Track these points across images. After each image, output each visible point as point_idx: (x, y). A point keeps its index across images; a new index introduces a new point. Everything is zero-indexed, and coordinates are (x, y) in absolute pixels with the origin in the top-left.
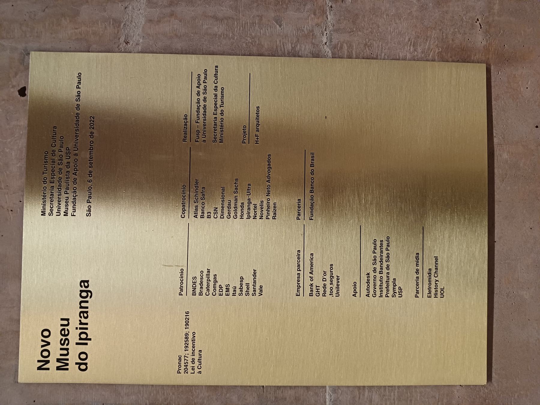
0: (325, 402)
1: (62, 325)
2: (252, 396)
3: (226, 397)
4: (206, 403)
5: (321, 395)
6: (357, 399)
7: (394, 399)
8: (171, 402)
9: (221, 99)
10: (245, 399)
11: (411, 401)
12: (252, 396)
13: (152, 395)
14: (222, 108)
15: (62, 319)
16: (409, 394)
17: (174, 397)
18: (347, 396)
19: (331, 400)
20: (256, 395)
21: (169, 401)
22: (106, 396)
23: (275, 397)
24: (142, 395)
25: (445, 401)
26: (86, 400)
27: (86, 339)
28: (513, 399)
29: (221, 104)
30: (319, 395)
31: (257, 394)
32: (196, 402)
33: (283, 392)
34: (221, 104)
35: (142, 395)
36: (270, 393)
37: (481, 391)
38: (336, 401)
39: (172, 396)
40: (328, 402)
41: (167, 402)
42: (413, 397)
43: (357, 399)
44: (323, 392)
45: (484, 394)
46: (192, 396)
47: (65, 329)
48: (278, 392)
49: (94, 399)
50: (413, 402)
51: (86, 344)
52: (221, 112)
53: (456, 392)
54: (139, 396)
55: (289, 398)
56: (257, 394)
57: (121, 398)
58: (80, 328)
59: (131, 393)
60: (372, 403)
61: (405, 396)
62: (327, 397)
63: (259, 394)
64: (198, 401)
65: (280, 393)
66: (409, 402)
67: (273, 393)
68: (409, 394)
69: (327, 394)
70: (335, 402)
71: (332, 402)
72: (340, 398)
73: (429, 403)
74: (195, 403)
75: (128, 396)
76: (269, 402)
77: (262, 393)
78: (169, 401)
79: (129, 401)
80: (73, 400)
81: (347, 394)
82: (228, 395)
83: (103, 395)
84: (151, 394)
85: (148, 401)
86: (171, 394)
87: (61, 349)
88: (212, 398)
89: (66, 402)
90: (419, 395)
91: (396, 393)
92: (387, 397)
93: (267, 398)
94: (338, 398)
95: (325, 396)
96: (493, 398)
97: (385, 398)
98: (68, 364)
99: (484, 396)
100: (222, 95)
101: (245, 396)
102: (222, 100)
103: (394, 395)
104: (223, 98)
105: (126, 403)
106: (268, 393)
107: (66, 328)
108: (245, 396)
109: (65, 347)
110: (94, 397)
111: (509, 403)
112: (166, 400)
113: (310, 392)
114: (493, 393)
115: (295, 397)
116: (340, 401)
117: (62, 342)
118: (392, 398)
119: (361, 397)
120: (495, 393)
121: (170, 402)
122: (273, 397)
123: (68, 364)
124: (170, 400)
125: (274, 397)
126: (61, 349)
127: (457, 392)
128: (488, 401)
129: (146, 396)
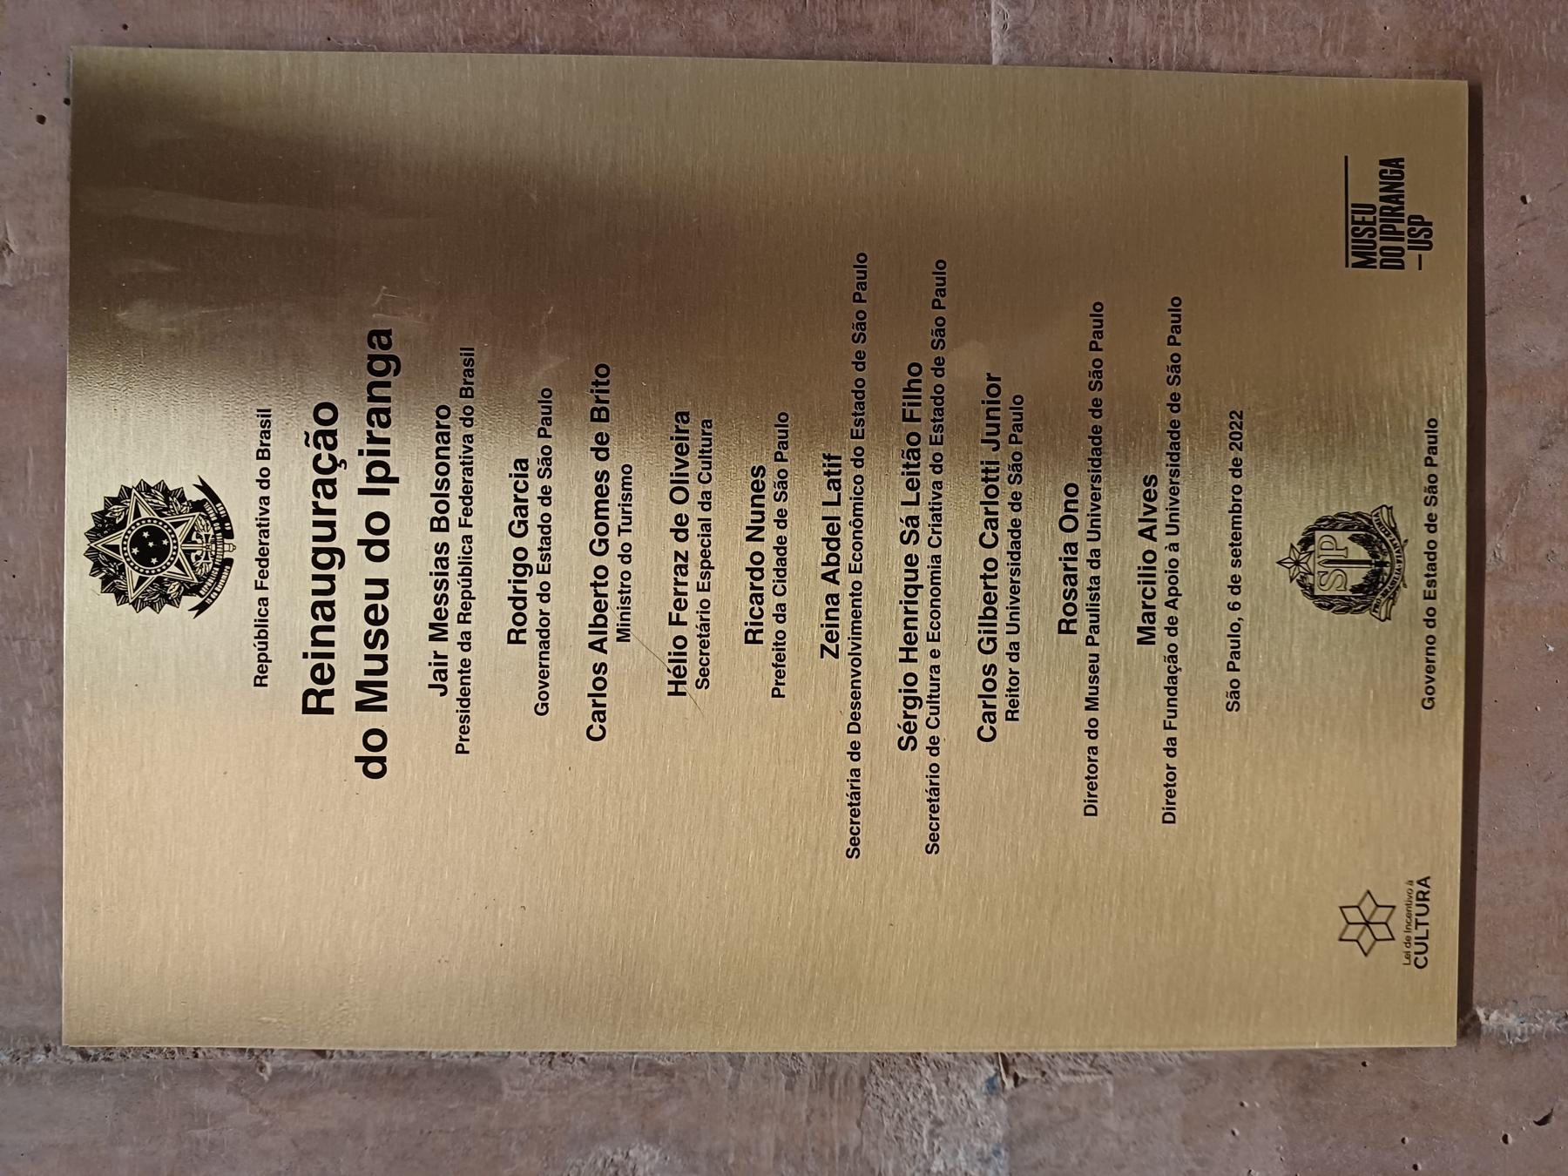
0: (988, 40)
1: (368, 597)
2: (771, 16)
3: (694, 17)
4: (635, 35)
5: (974, 18)
6: (1083, 25)
7: (1192, 29)
8: (530, 32)
9: (624, 505)
10: (748, 24)
11: (1242, 36)
12: (771, 16)
13: (473, 11)
14: (626, 537)
15: (369, 582)
16: (1235, 13)
17: (537, 18)
18: (1052, 14)
19: (1005, 26)
20: (782, 12)
21: (523, 28)
22: (336, 17)
23: (838, 20)
24: (442, 13)
25: (1344, 37)
26: (277, 25)
27: (386, 479)
28: (1544, 33)
29: (623, 524)
30: (970, 18)
31: (786, 11)
32: (603, 31)
33: (861, 6)
34: (623, 524)
35: (442, 13)
36: (825, 10)
37: (1451, 11)
38: (1020, 27)
39: (533, 15)
40: (995, 36)
41: (518, 32)
42: (1248, 24)
43: (1083, 25)
44: (982, 12)
45: (1459, 19)
46: (593, 15)
47: (377, 605)
48: (846, 8)
49: (302, 25)
50: (1249, 39)
51: (386, 492)
52: (623, 550)
53: (1376, 13)
54: (436, 16)
55: (881, 23)
56: (786, 11)
57: (380, 22)
58: (370, 453)
59: (412, 8)
60: (1129, 36)
61: (1224, 19)
62: (994, 23)
63: (791, 11)
64: (610, 29)
65: (853, 9)
66: (1236, 38)
67: (834, 9)
68: (1235, 13)
69: (993, 14)
70: (1017, 32)
71: (1009, 32)
72: (1033, 20)
73: (1296, 43)
74: (600, 33)
75: (401, 15)
76: (821, 36)
77: (800, 9)
78: (523, 28)
79: (405, 30)
80: (238, 26)
81: (1054, 10)
82: (699, 12)
83: (327, 13)
84: (470, 11)
85: (460, 31)
86: (529, 9)
87: (368, 657)
88: (651, 20)
89: (217, 32)
90: (1265, 19)
91: (1198, 13)
92: (1171, 23)
93: (816, 24)
94: (1027, 20)
95: (988, 22)
96: (1486, 29)
97: (1165, 23)
98: (386, 694)
99: (1461, 24)
100: (626, 492)
101: (748, 17)
102: (626, 509)
103: (1193, 16)
104: (627, 502)
105: (397, 35)
106: (817, 9)
107: (379, 603)
108: (748, 17)
109: (377, 651)
110: (300, 20)
111: (1533, 46)
112: (514, 26)
113: (941, 10)
114: (1487, 16)
115: (897, 23)
116: (1032, 28)
117: (371, 639)
118: (1187, 24)
119: (1094, 20)
120: (1492, 15)
121: (526, 33)
122: (832, 22)
123: (386, 694)
124: (527, 26)
125: (835, 21)
126: (368, 657)
127: (1381, 11)
128: (1471, 41)
129: (454, 15)
